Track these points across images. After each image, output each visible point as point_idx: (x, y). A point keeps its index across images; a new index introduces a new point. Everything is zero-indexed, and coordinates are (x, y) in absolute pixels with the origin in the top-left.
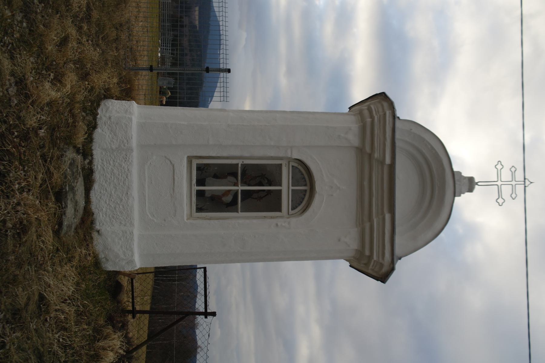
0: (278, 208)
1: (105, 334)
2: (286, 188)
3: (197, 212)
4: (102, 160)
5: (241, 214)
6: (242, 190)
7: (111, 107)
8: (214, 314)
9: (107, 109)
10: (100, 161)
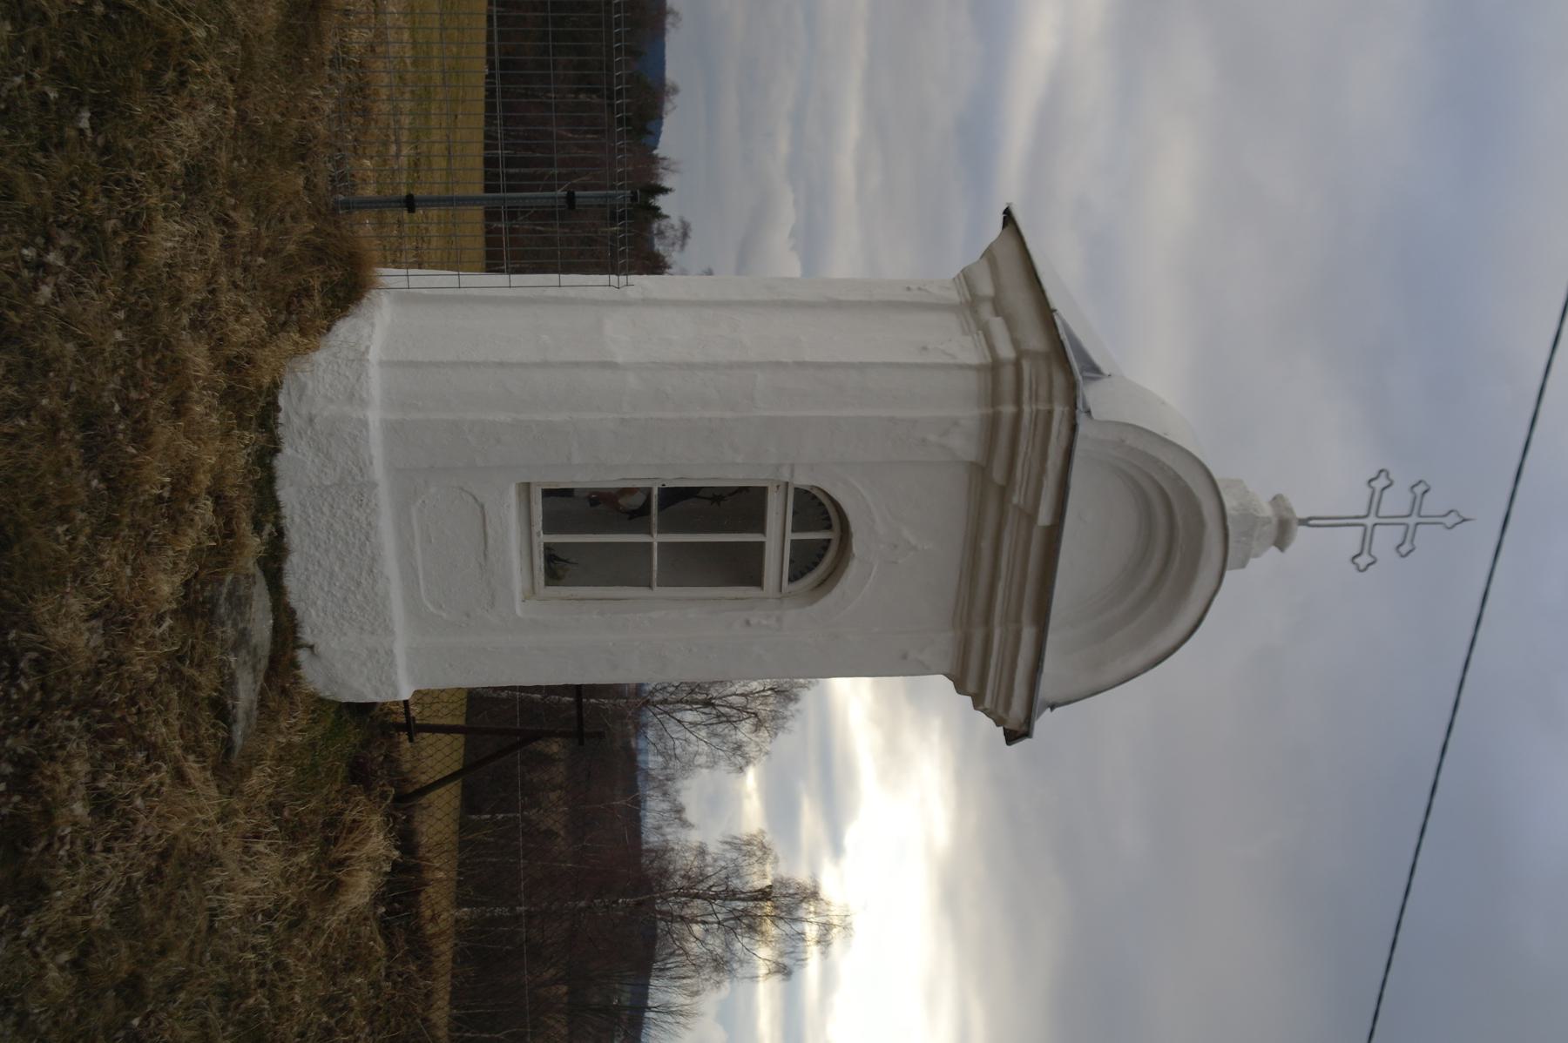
0: (756, 580)
1: (348, 823)
2: (777, 537)
3: (547, 584)
4: (303, 505)
5: (658, 591)
7: (310, 385)
9: (302, 389)
10: (298, 506)
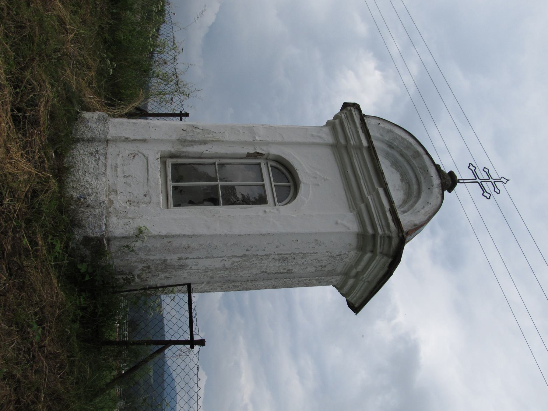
6: (222, 186)
8: (202, 343)
